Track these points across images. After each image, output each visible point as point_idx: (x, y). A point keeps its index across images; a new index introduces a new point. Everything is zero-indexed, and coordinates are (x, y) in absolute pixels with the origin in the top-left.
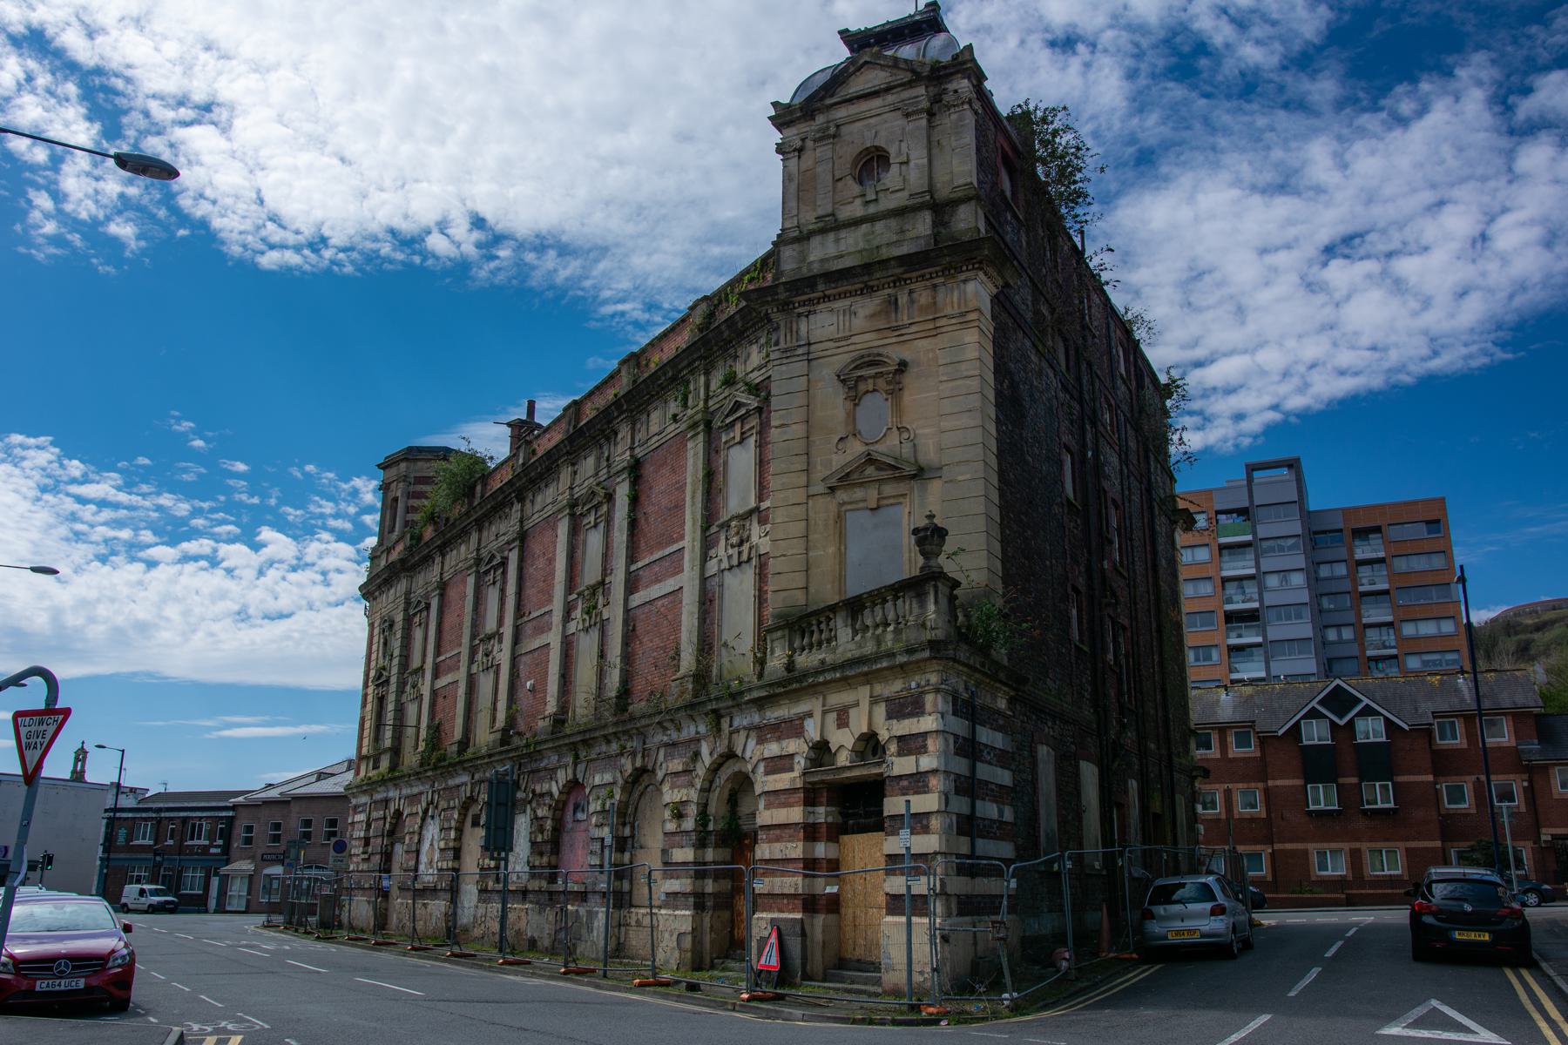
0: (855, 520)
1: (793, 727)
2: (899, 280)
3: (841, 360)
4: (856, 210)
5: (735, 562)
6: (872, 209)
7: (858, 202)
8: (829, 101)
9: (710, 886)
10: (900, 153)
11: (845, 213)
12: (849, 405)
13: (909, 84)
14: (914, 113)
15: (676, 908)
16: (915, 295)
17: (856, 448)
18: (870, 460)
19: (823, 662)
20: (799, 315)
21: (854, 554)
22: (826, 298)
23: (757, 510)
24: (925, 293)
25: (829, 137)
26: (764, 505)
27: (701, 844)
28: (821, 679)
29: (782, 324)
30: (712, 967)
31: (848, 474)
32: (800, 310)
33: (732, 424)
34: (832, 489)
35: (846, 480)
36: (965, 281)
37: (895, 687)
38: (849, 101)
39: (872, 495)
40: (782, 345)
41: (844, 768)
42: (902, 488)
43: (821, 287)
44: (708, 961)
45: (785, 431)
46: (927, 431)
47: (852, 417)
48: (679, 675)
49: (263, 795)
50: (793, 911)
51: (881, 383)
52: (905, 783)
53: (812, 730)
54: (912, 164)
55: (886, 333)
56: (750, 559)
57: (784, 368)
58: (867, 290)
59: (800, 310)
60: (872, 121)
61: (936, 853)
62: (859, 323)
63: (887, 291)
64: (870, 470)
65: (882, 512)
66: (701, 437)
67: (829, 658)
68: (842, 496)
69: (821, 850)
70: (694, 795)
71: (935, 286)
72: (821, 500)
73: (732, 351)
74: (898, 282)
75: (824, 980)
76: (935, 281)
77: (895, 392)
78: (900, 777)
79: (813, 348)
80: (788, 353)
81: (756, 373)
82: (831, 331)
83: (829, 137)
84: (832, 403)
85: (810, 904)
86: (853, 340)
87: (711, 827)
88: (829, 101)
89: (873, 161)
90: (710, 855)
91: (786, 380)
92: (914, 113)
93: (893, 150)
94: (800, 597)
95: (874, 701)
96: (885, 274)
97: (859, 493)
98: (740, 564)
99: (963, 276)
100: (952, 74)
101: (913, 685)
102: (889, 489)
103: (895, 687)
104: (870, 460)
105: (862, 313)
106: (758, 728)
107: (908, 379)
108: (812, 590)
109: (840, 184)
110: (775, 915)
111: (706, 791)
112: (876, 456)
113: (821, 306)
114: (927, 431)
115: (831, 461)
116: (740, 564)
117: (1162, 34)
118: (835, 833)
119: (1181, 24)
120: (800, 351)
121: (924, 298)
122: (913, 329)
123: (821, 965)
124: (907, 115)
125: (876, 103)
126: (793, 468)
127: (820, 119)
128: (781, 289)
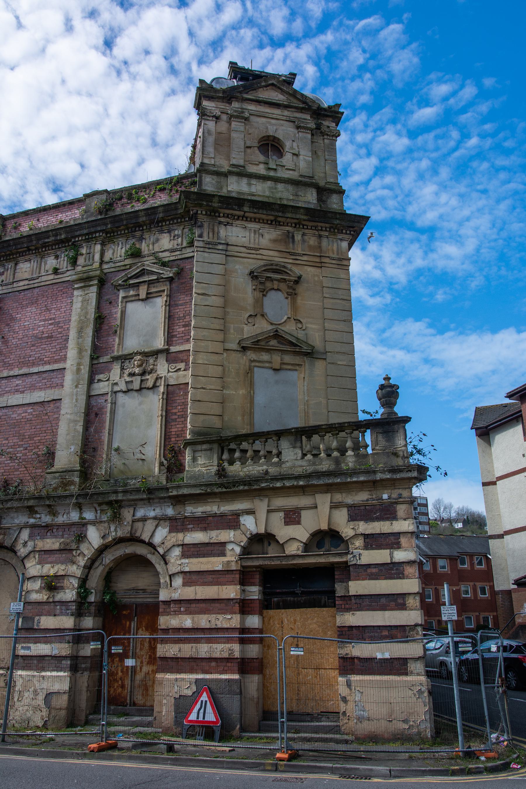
0: (261, 375)
1: (232, 522)
2: (299, 224)
3: (253, 264)
4: (261, 170)
5: (136, 385)
6: (272, 174)
7: (262, 166)
8: (246, 96)
9: (89, 649)
10: (292, 148)
11: (252, 169)
12: (258, 294)
13: (301, 110)
14: (304, 128)
15: (43, 669)
16: (306, 238)
17: (262, 327)
18: (276, 335)
19: (267, 473)
20: (220, 223)
21: (260, 398)
22: (244, 218)
23: (166, 351)
24: (313, 239)
25: (243, 118)
26: (173, 349)
27: (79, 614)
28: (278, 485)
29: (206, 225)
30: (87, 723)
31: (258, 341)
32: (222, 220)
33: (137, 286)
34: (244, 349)
35: (257, 345)
36: (341, 240)
37: (361, 497)
38: (258, 102)
39: (277, 359)
40: (205, 238)
41: (294, 556)
42: (297, 360)
43: (246, 209)
44: (83, 717)
45: (197, 302)
46: (314, 326)
47: (259, 303)
48: (53, 470)
49: (300, 561)
50: (233, 673)
51: (283, 286)
52: (374, 570)
53: (250, 524)
54: (301, 157)
55: (285, 255)
56: (155, 386)
57: (206, 255)
58: (275, 223)
59: (222, 220)
60: (273, 121)
61: (416, 625)
62: (264, 242)
63: (287, 228)
64: (273, 343)
65: (283, 375)
66: (94, 289)
67: (273, 470)
68: (252, 355)
69: (254, 621)
70: (76, 570)
71: (320, 236)
72: (234, 355)
73: (138, 234)
74: (298, 225)
75: (259, 731)
76: (322, 233)
77: (292, 295)
78: (369, 566)
79: (230, 248)
80: (210, 246)
81: (167, 254)
82: (244, 241)
83: (243, 118)
84: (245, 290)
85: (244, 666)
86: (261, 252)
87: (92, 598)
88: (246, 96)
89: (271, 145)
90: (88, 622)
91: (203, 265)
92: (304, 128)
93: (288, 144)
94: (216, 423)
95: (335, 506)
96: (294, 216)
97: (265, 357)
98: (141, 389)
99: (340, 236)
100: (327, 116)
101: (385, 496)
102: (288, 358)
103: (361, 497)
104: (276, 335)
105: (267, 236)
106: (171, 519)
107: (301, 289)
108: (226, 418)
109: (249, 150)
110: (200, 676)
111: (89, 567)
112: (281, 333)
113: (238, 222)
114: (314, 326)
115: (243, 330)
116: (141, 389)
117: (9, 203)
118: (266, 605)
119: (20, 201)
120: (220, 247)
121: (312, 241)
122: (305, 258)
123: (258, 715)
124: (298, 127)
125: (277, 112)
126: (212, 326)
127: (235, 105)
128: (216, 199)
